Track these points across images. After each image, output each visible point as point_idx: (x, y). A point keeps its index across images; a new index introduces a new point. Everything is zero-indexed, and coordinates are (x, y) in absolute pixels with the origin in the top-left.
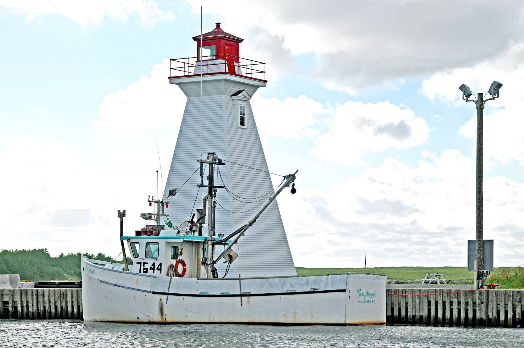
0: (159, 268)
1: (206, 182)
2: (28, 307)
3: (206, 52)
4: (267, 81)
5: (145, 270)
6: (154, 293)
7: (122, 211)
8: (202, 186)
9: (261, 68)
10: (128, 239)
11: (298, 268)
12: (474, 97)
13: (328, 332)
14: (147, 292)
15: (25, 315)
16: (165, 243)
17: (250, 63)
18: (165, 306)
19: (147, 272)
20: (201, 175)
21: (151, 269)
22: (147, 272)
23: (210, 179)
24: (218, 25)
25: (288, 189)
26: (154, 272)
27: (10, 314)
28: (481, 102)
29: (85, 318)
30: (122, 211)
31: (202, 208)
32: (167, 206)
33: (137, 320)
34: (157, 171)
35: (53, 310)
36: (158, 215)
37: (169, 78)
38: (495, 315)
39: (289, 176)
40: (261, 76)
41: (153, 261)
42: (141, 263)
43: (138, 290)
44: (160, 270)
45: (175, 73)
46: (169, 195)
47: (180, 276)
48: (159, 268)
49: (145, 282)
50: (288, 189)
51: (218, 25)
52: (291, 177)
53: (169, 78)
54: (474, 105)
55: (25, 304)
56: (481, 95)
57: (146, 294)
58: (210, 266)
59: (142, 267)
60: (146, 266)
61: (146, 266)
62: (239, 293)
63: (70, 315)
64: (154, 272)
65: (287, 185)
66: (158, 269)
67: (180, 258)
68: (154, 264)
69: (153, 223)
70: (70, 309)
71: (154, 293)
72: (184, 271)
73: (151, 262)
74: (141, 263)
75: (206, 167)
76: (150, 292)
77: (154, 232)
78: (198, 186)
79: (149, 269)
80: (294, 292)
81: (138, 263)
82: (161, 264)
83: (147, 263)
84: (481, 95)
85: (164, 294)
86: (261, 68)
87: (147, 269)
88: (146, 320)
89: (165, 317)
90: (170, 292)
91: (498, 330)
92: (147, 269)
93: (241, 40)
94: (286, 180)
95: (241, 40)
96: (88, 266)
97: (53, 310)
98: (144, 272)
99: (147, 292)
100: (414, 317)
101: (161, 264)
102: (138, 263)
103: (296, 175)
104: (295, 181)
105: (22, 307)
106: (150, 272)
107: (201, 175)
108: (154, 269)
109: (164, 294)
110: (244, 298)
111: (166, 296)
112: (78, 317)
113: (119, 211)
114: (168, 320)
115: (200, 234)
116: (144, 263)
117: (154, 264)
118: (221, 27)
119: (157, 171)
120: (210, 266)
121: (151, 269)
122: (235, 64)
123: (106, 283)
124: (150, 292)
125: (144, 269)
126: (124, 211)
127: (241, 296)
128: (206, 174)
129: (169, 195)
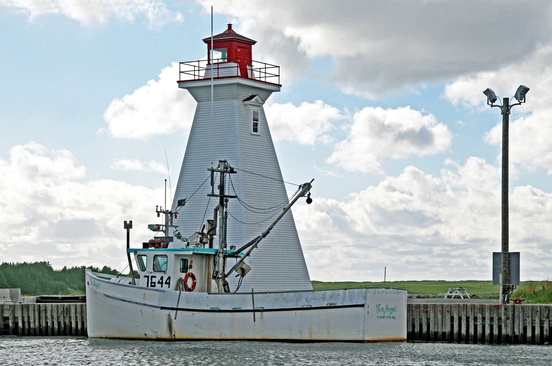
0: (168, 281)
1: (217, 192)
2: (29, 323)
3: (217, 55)
4: (281, 86)
5: (153, 284)
6: (162, 308)
7: (128, 222)
8: (213, 195)
9: (275, 71)
10: (135, 251)
11: (314, 282)
12: (499, 102)
13: (346, 349)
14: (155, 307)
15: (26, 331)
16: (173, 256)
17: (263, 66)
18: (174, 322)
19: (154, 286)
20: (212, 184)
21: (159, 283)
22: (154, 286)
23: (222, 188)
24: (230, 26)
25: (304, 199)
26: (162, 287)
27: (11, 330)
28: (506, 108)
29: (89, 334)
30: (128, 222)
31: (213, 219)
32: (176, 217)
33: (144, 336)
34: (166, 180)
35: (56, 326)
36: (166, 226)
37: (178, 82)
38: (522, 331)
39: (305, 185)
40: (275, 80)
41: (161, 274)
42: (148, 277)
43: (145, 305)
44: (169, 284)
45: (184, 77)
46: (178, 206)
47: (190, 290)
48: (168, 281)
49: (153, 298)
50: (304, 199)
51: (230, 26)
52: (307, 186)
53: (178, 82)
54: (499, 110)
55: (26, 320)
56: (506, 100)
57: (154, 309)
58: (221, 280)
59: (150, 281)
60: (154, 280)
61: (154, 280)
62: (252, 309)
63: (74, 332)
64: (162, 287)
65: (302, 195)
66: (166, 283)
67: (190, 271)
68: (162, 278)
69: (161, 234)
70: (74, 325)
71: (162, 308)
72: (194, 285)
73: (159, 275)
74: (148, 277)
75: (217, 175)
76: (158, 307)
77: (162, 244)
78: (208, 195)
79: (157, 283)
80: (309, 307)
81: (146, 276)
82: (169, 278)
83: (155, 277)
84: (506, 100)
85: (172, 309)
86: (275, 71)
87: (155, 283)
88: (154, 337)
89: (173, 333)
90: (180, 307)
91: (525, 347)
92: (155, 283)
93: (254, 43)
94: (301, 190)
95: (254, 43)
96: (93, 280)
97: (56, 326)
98: (152, 286)
99: (155, 307)
100: (436, 333)
101: (169, 278)
102: (146, 276)
103: (311, 184)
104: (311, 191)
105: (23, 323)
106: (158, 286)
107: (212, 184)
108: (162, 283)
109: (172, 309)
110: (258, 314)
111: (174, 312)
112: (82, 333)
113: (125, 222)
114: (178, 336)
115: (211, 246)
116: (152, 277)
117: (162, 278)
118: (233, 28)
119: (166, 180)
120: (221, 280)
121: (159, 283)
122: (248, 67)
123: (111, 297)
124: (158, 307)
125: (152, 283)
126: (131, 222)
127: (254, 311)
128: (217, 183)
129: (178, 206)
